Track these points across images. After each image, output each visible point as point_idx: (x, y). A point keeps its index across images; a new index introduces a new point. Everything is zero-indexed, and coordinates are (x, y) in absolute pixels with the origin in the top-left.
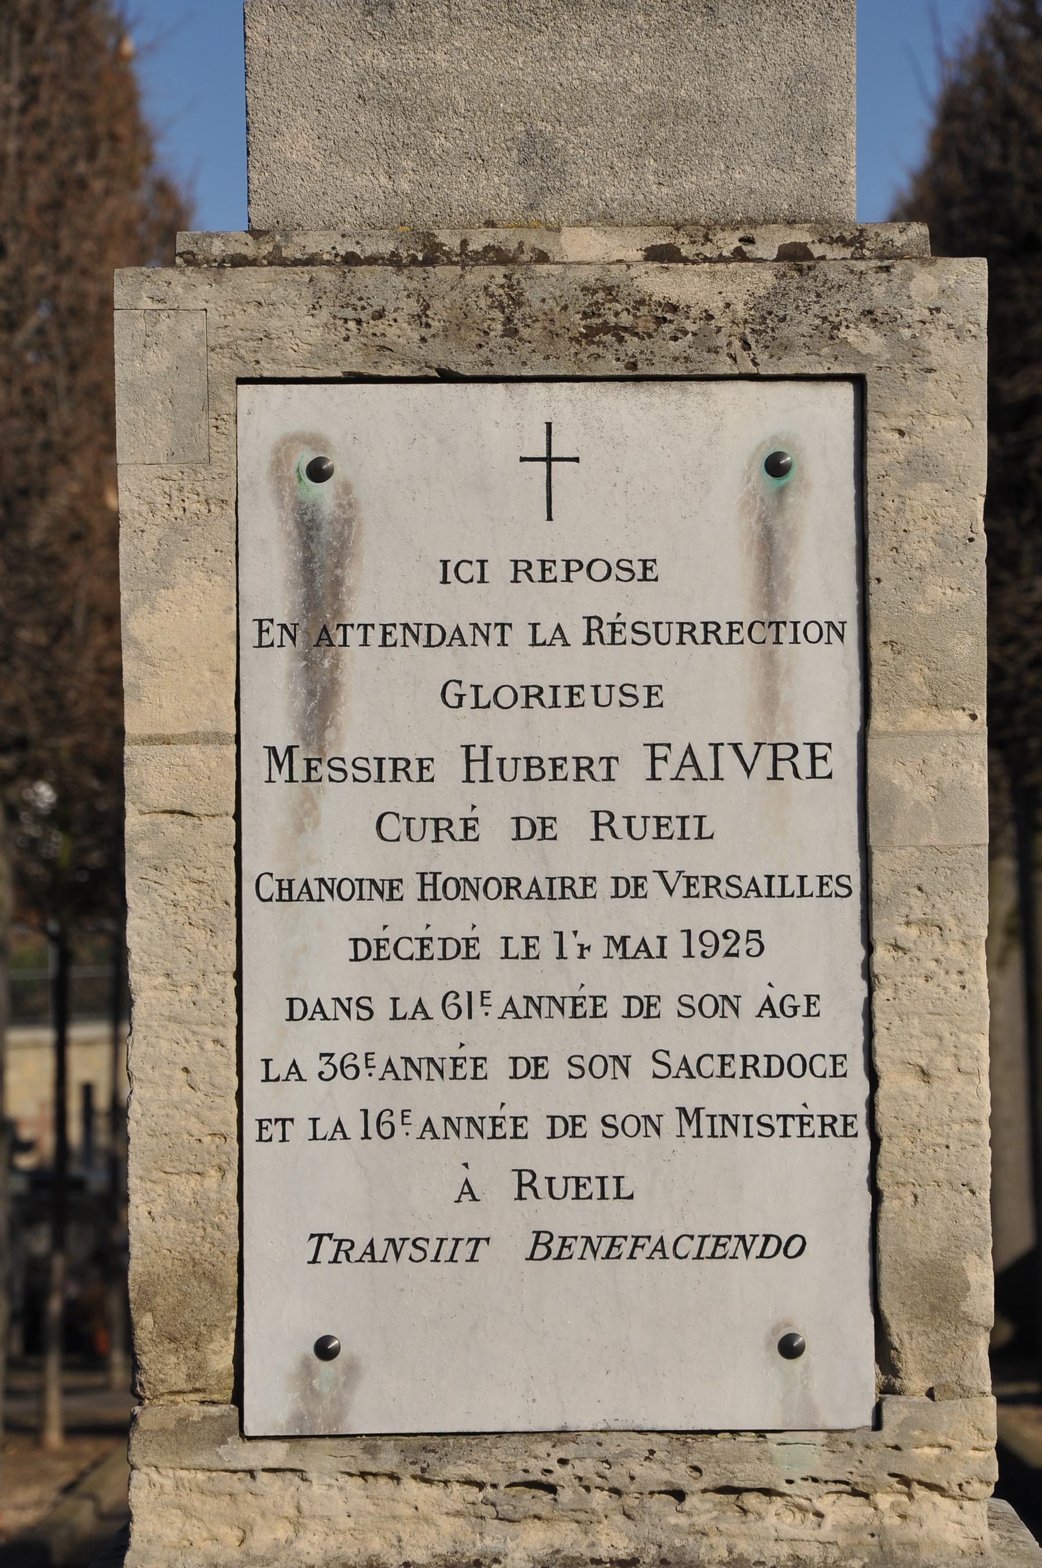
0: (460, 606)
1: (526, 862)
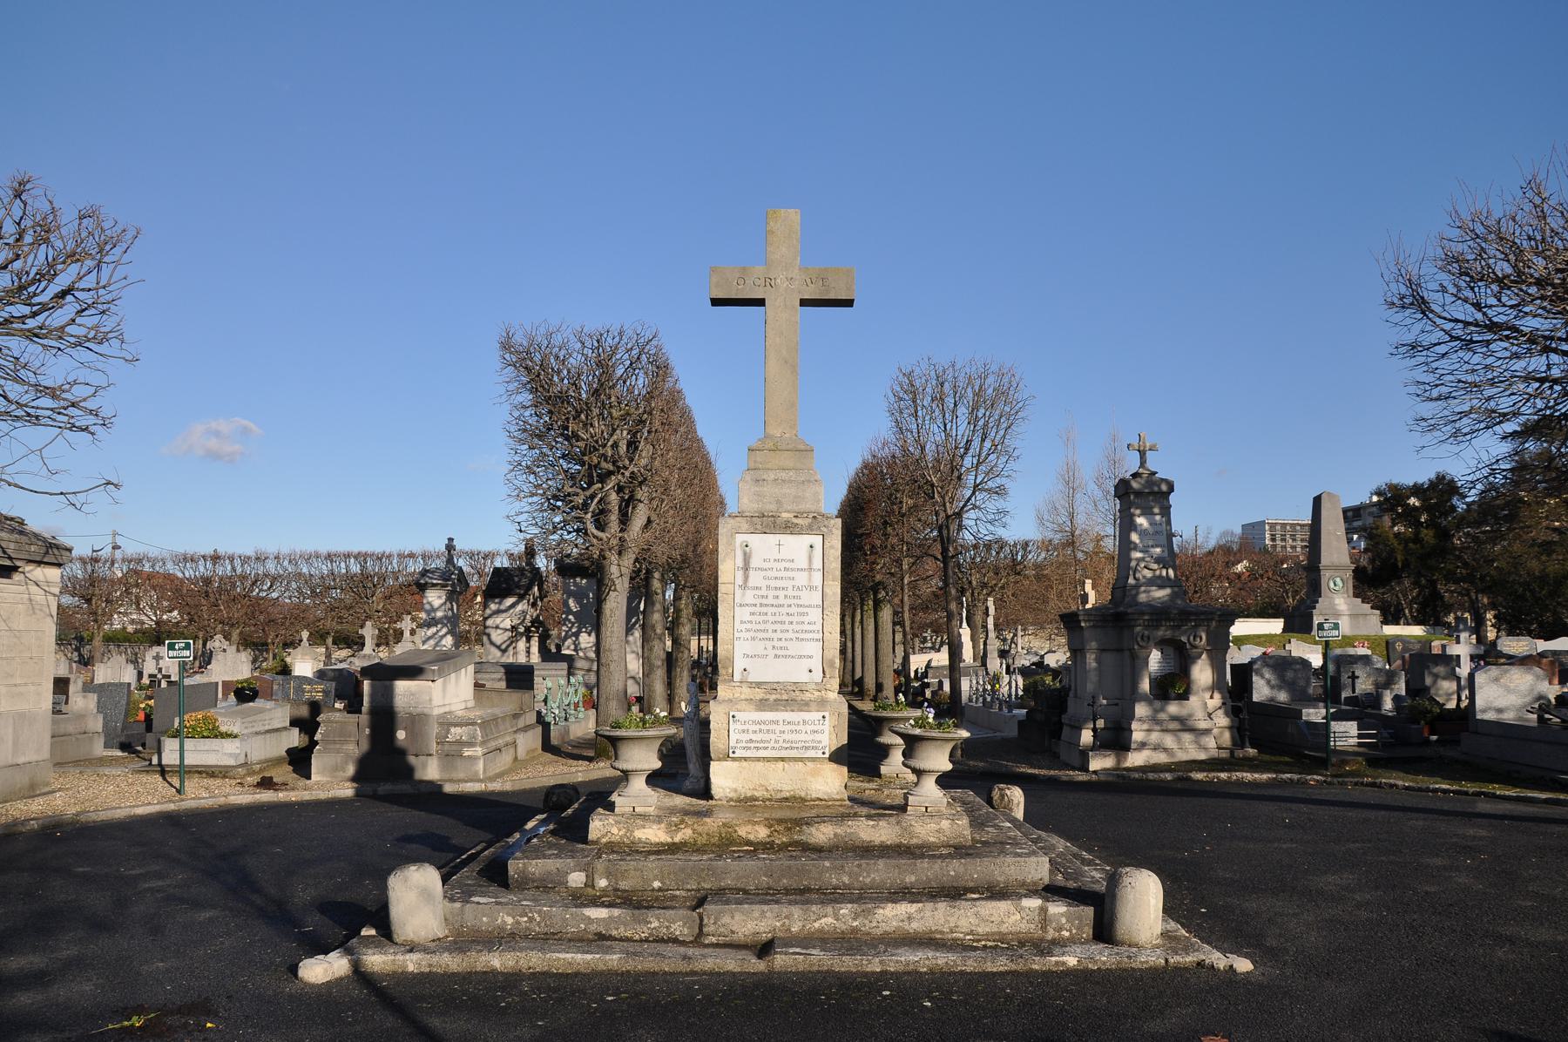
0: (766, 565)
1: (775, 602)
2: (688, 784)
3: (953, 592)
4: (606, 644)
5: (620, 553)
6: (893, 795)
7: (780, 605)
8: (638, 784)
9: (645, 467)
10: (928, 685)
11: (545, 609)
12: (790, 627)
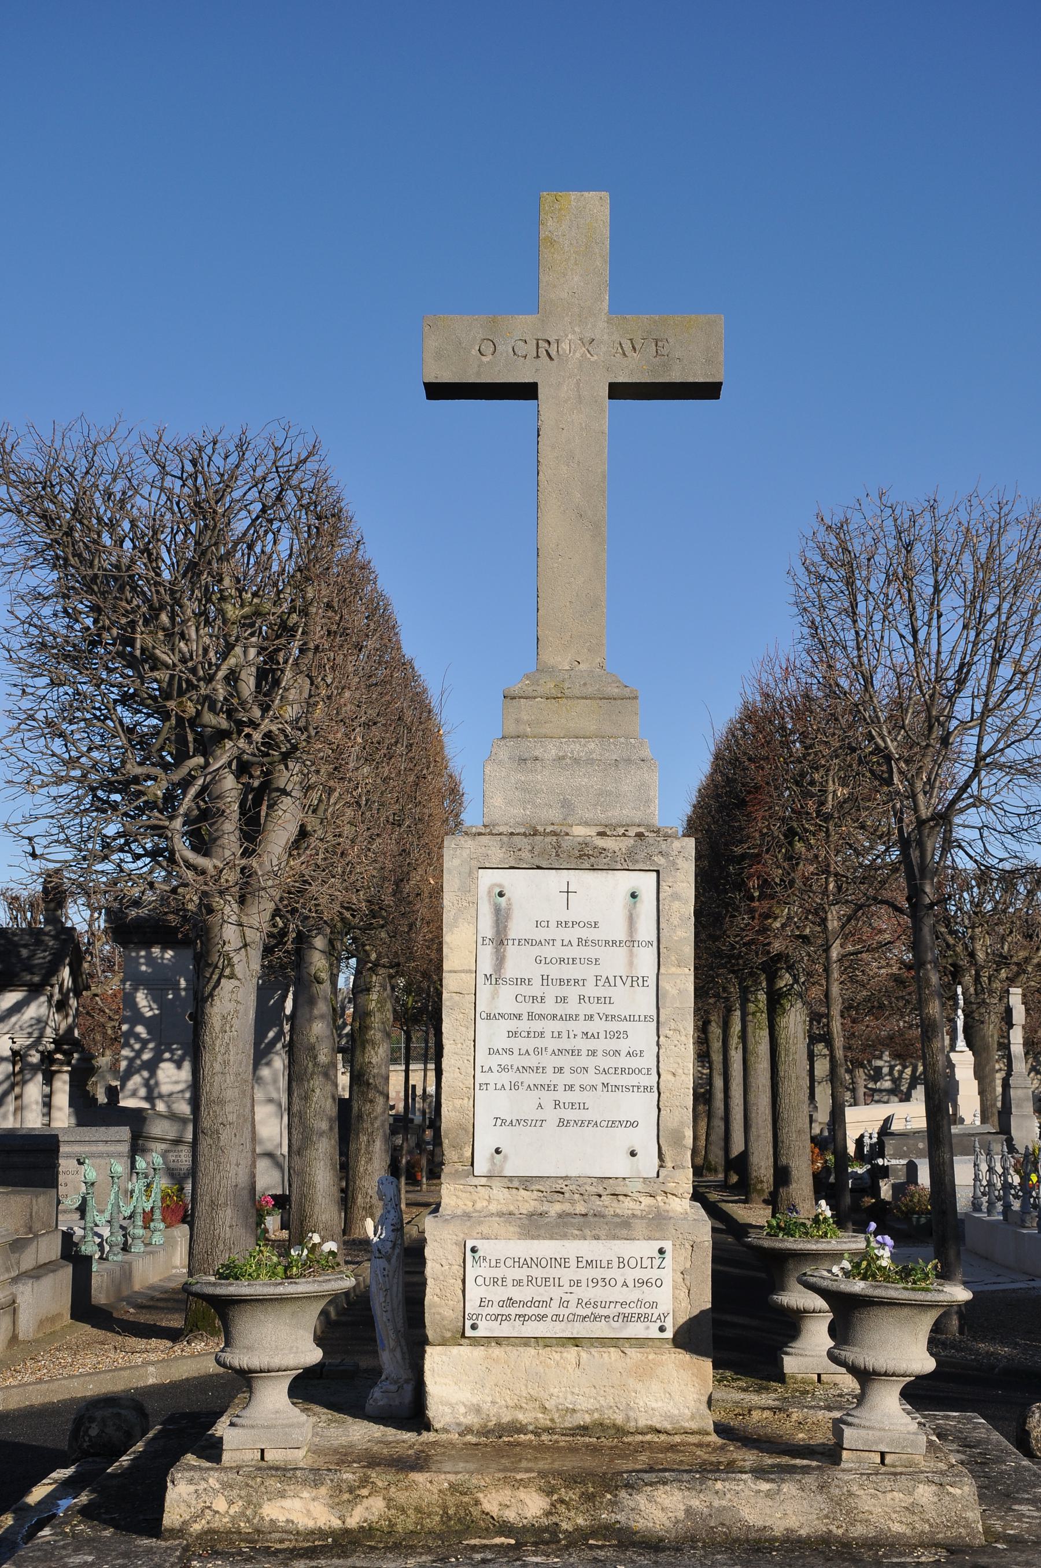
0: (541, 934)
1: (559, 1010)
2: (378, 1396)
3: (934, 978)
4: (212, 1087)
5: (242, 901)
6: (809, 1423)
7: (569, 1021)
8: (273, 1399)
9: (295, 723)
10: (884, 1172)
11: (86, 1012)
12: (590, 1062)
